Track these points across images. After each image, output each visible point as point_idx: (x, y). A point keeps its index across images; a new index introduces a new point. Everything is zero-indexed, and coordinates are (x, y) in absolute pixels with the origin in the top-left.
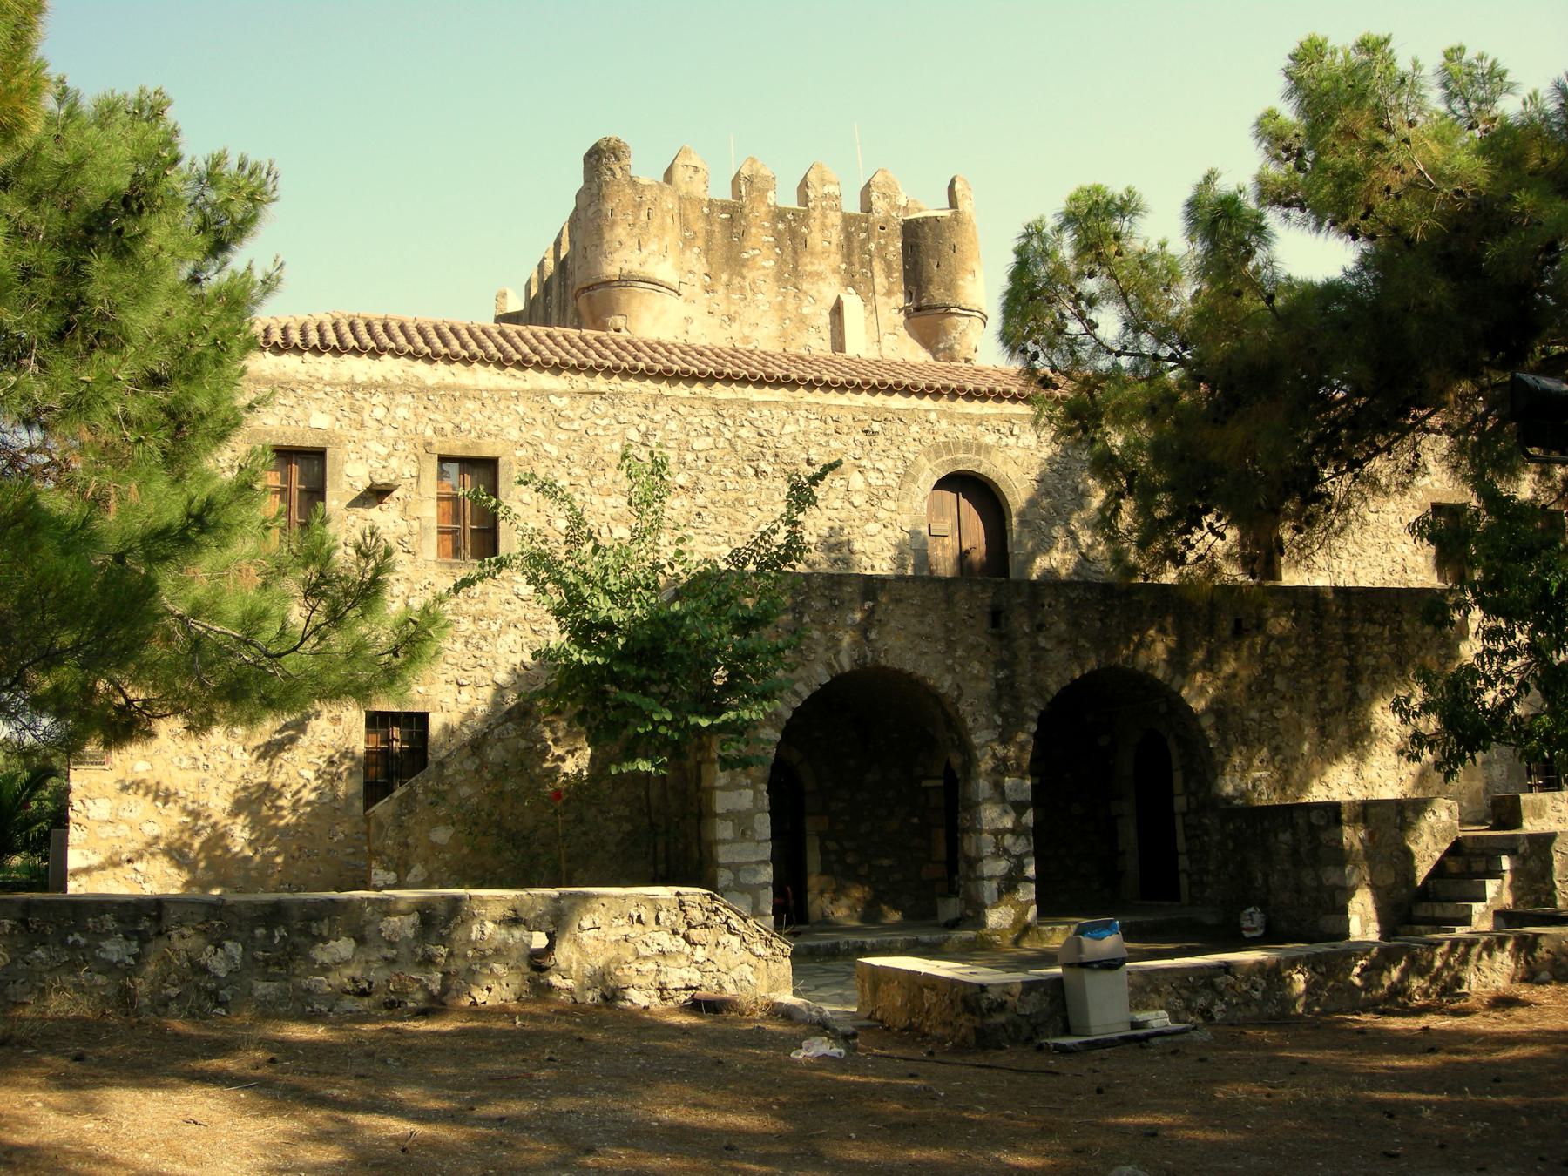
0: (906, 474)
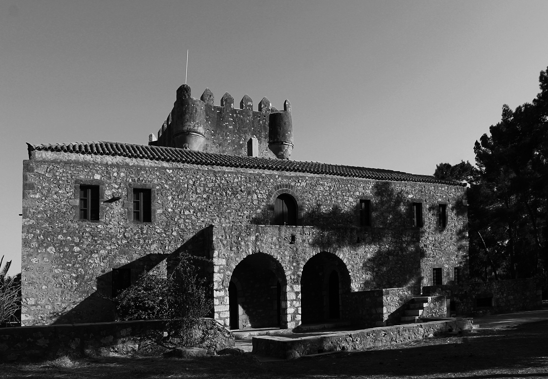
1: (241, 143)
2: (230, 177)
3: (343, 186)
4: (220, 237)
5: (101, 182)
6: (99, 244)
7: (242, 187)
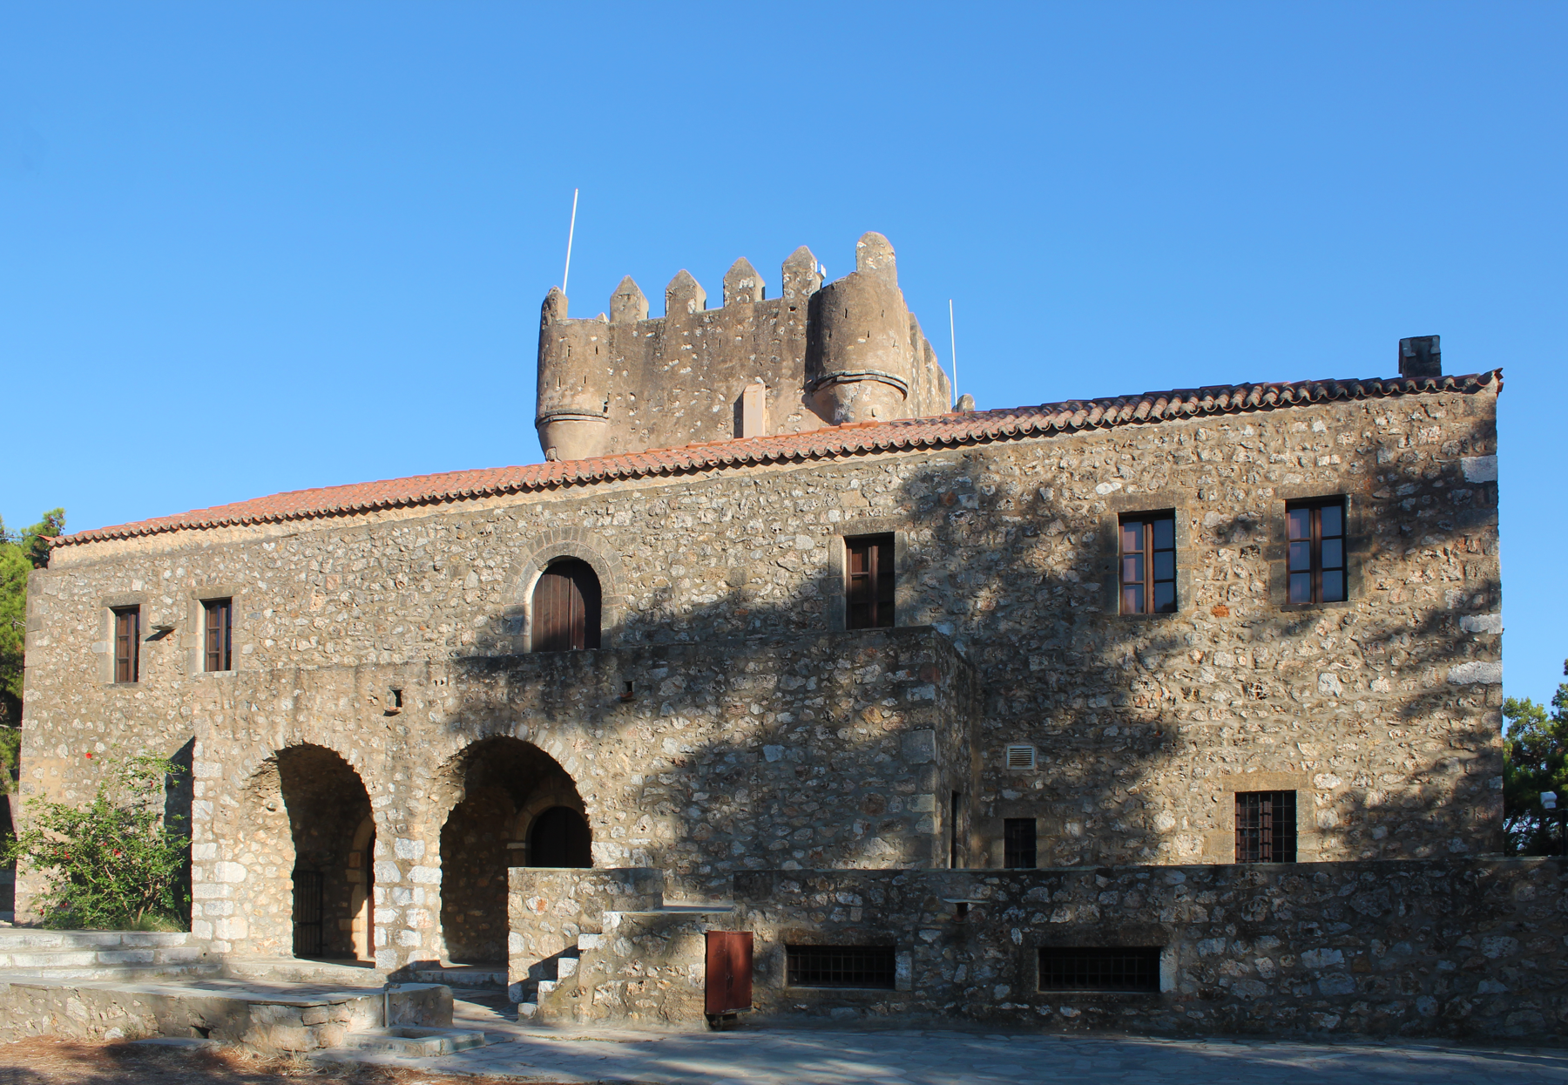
0: (512, 567)
1: (715, 409)
2: (407, 536)
3: (774, 498)
4: (211, 707)
5: (145, 596)
6: (137, 735)
7: (437, 558)
